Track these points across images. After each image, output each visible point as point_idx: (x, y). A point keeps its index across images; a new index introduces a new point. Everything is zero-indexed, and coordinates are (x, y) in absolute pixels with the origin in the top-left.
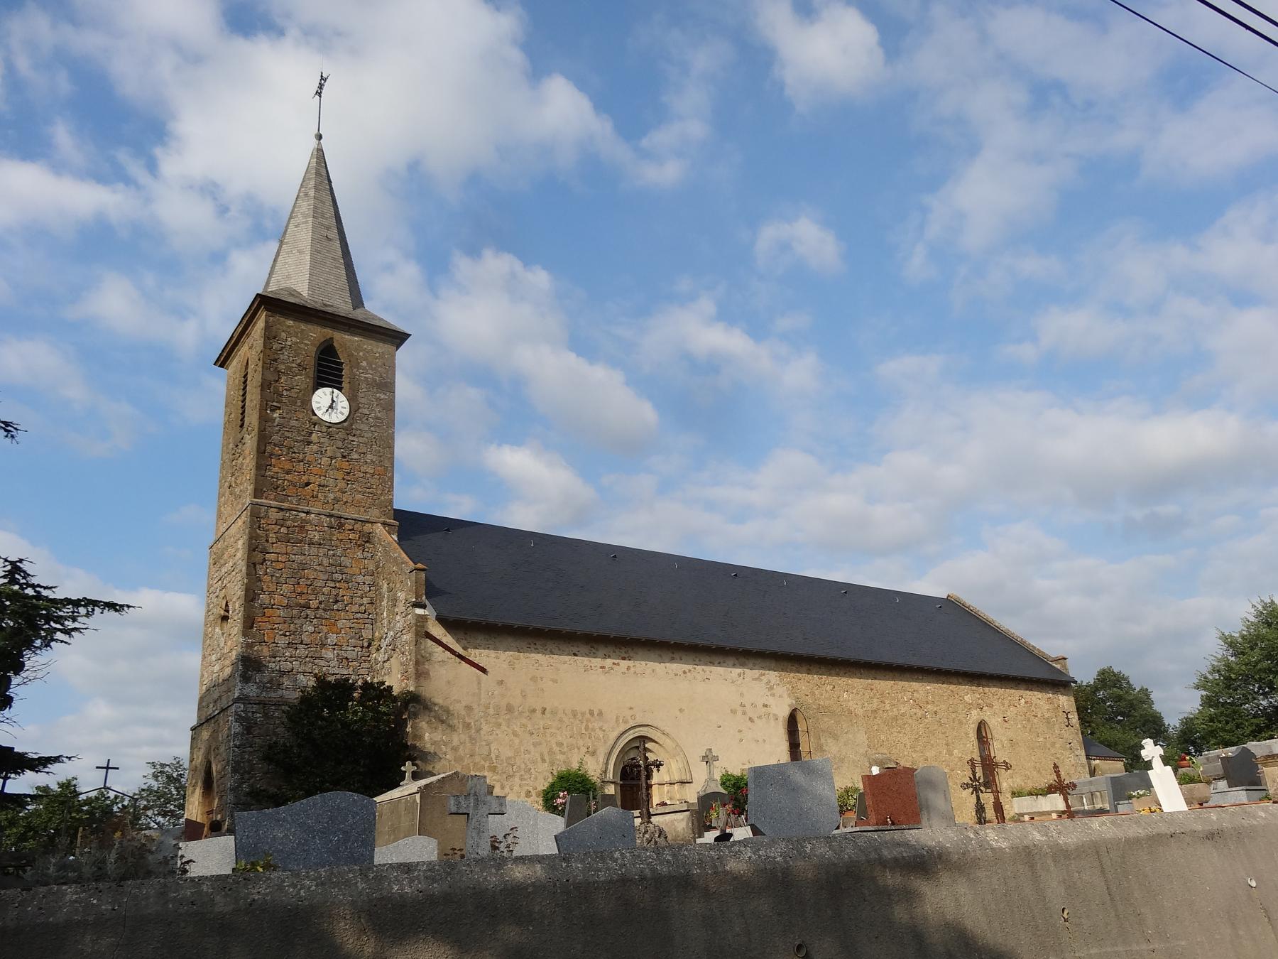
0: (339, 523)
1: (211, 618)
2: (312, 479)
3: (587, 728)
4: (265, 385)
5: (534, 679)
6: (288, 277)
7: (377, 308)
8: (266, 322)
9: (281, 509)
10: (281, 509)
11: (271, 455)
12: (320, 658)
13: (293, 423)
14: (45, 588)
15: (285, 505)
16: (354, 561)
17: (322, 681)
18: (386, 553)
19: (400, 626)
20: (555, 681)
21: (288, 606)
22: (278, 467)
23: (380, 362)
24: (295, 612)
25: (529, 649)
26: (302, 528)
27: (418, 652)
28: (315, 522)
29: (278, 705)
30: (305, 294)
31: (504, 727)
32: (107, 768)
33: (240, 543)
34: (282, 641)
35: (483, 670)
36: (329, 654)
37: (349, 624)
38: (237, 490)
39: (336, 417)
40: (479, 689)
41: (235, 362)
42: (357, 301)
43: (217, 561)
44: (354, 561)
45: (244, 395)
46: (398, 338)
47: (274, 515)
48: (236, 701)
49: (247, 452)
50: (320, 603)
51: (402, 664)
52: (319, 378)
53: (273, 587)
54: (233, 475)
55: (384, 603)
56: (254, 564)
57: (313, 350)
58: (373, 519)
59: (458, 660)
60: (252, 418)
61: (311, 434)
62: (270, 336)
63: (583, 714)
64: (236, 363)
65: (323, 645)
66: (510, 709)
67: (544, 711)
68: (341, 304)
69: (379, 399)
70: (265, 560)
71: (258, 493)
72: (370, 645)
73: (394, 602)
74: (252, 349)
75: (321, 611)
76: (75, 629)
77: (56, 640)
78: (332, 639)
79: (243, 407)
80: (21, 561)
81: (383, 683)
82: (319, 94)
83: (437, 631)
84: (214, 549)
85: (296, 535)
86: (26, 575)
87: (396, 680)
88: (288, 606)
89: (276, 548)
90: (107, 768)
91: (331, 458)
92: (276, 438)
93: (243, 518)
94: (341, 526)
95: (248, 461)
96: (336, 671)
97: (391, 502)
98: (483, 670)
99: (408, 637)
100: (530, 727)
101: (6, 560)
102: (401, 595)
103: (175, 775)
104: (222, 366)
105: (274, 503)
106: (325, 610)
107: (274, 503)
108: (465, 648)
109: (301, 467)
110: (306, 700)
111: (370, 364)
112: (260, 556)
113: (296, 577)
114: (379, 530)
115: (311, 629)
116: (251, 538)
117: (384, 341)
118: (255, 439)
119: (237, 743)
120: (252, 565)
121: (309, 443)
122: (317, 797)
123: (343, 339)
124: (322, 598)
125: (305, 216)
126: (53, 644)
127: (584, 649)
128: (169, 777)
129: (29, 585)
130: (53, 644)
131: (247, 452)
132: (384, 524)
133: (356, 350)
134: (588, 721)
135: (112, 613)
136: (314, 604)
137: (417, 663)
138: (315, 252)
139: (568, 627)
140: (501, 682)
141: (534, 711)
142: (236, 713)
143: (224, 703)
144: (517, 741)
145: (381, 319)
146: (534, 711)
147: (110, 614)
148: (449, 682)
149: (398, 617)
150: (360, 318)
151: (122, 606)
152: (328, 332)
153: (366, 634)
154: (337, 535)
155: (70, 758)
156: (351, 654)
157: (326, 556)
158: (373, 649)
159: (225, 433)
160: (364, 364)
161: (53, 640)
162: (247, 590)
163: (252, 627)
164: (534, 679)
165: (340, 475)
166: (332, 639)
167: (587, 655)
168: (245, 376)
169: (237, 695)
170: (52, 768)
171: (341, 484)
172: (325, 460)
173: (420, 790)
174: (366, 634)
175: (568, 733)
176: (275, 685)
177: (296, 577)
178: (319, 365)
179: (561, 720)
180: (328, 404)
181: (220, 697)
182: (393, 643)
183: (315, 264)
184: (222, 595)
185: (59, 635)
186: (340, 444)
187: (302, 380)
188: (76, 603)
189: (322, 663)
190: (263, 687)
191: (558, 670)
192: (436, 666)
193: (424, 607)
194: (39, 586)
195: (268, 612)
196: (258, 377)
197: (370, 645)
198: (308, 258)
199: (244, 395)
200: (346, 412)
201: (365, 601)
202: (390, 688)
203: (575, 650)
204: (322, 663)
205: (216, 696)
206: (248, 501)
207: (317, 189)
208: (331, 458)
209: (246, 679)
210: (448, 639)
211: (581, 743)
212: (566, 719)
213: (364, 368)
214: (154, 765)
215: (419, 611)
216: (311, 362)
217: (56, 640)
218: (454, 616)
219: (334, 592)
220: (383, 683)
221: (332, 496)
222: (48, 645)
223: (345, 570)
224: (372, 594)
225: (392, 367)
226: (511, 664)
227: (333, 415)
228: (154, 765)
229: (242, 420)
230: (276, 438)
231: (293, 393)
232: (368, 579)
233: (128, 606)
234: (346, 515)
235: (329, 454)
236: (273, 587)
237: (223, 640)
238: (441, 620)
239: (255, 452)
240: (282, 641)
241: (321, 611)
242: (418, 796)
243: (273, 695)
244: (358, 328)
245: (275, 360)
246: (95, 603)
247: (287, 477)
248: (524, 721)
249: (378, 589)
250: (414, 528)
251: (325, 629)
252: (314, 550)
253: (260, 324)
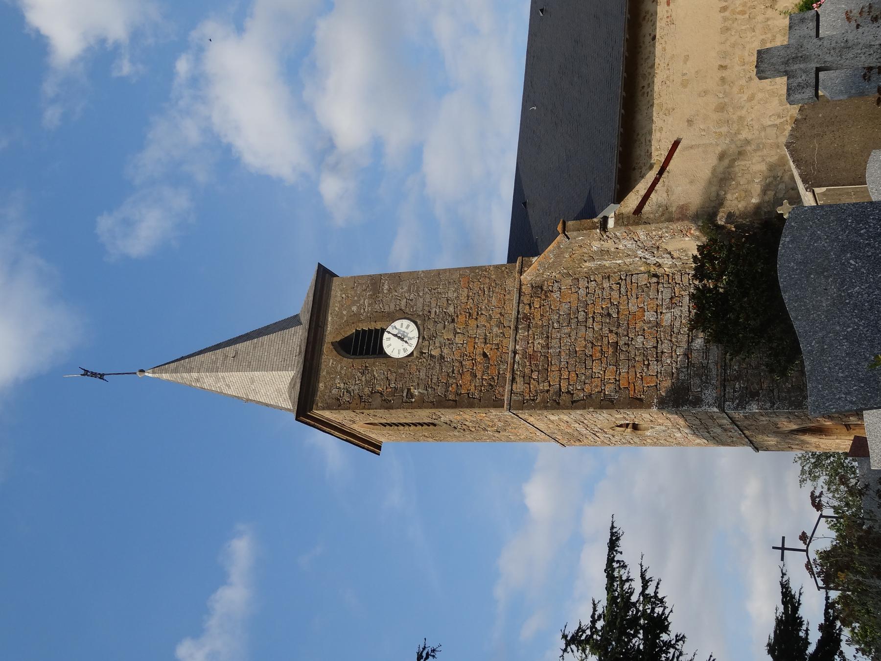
0: (523, 320)
1: (636, 440)
2: (479, 351)
3: (743, 13)
4: (387, 405)
5: (684, 84)
6: (279, 391)
7: (297, 300)
8: (323, 409)
9: (513, 380)
10: (513, 380)
11: (458, 394)
12: (672, 326)
13: (422, 375)
14: (595, 610)
15: (508, 376)
16: (563, 300)
17: (696, 323)
18: (551, 266)
19: (630, 244)
20: (687, 58)
21: (616, 365)
22: (469, 385)
23: (351, 293)
24: (622, 357)
25: (649, 94)
26: (531, 357)
27: (657, 221)
28: (524, 343)
29: (725, 367)
30: (292, 374)
31: (743, 113)
32: (783, 549)
33: (552, 418)
34: (655, 367)
35: (676, 144)
36: (667, 318)
37: (633, 300)
38: (500, 424)
39: (411, 330)
40: (698, 146)
41: (373, 436)
42: (294, 321)
43: (577, 439)
44: (563, 300)
45: (402, 425)
46: (324, 276)
47: (519, 386)
48: (723, 410)
49: (459, 418)
50: (611, 331)
51: (673, 237)
52: (374, 353)
53: (597, 382)
54: (485, 430)
55: (607, 263)
56: (573, 402)
57: (347, 361)
58: (517, 285)
59: (665, 175)
60: (423, 415)
61: (432, 356)
62: (337, 405)
63: (725, 19)
64: (374, 435)
65: (658, 325)
66: (721, 108)
67: (722, 67)
68: (297, 336)
69: (389, 290)
70: (568, 392)
71: (497, 404)
72: (655, 276)
73: (603, 252)
74: (358, 422)
75: (620, 331)
76: (643, 576)
77: (656, 593)
78: (650, 316)
79: (415, 425)
80: (565, 636)
81: (695, 257)
82: (101, 376)
83: (632, 201)
84: (564, 442)
85: (539, 362)
86: (581, 630)
87: (687, 244)
88: (616, 365)
89: (554, 381)
90: (783, 549)
91: (456, 333)
92: (440, 390)
93: (526, 416)
94: (526, 318)
95: (468, 416)
96: (685, 309)
97: (497, 267)
98: (676, 144)
99: (641, 232)
100: (743, 82)
101: (565, 650)
102: (596, 245)
103: (813, 461)
104: (379, 448)
105: (508, 387)
106: (619, 326)
107: (508, 387)
108: (651, 167)
109: (467, 363)
110: (716, 338)
111: (354, 303)
112: (565, 398)
113: (585, 359)
114: (527, 277)
115: (640, 339)
116: (546, 408)
117: (330, 289)
118: (443, 411)
119: (768, 405)
120: (575, 404)
121: (442, 357)
122: (785, 296)
123: (333, 332)
124: (606, 331)
125: (218, 380)
126: (660, 596)
127: (646, 29)
128: (815, 465)
129: (593, 627)
130: (660, 596)
131: (459, 418)
132: (521, 272)
133: (341, 318)
134: (733, 12)
135: (621, 542)
136: (612, 338)
137: (670, 220)
138: (250, 367)
139: (621, 49)
140: (690, 122)
141: (723, 79)
142: (736, 409)
143: (726, 422)
144: (760, 95)
145: (308, 296)
146: (723, 79)
147: (623, 545)
148: (691, 182)
149: (621, 247)
150: (308, 316)
151: (612, 534)
152: (327, 348)
153: (643, 280)
154: (537, 321)
155: (784, 574)
156: (667, 294)
157: (559, 329)
158: (660, 271)
159: (444, 439)
160: (354, 308)
161: (656, 596)
162: (601, 407)
163: (641, 400)
164: (684, 84)
165: (473, 323)
166: (650, 316)
167: (654, 24)
168: (384, 425)
169: (716, 410)
170: (794, 589)
171: (482, 321)
172: (459, 340)
173: (810, 188)
174: (643, 280)
175: (749, 34)
176: (702, 372)
177: (585, 359)
178: (361, 354)
179: (733, 46)
180: (400, 341)
181: (720, 426)
182: (650, 250)
183: (261, 366)
184: (611, 432)
185: (650, 591)
186: (440, 326)
187: (378, 369)
188: (611, 578)
189: (677, 324)
190: (705, 384)
191: (673, 56)
192: (673, 198)
193: (605, 219)
194: (593, 616)
195: (623, 384)
196: (380, 412)
197: (655, 276)
198: (257, 373)
199: (402, 425)
200: (406, 322)
201: (606, 285)
202: (700, 248)
203: (648, 39)
204: (677, 324)
205: (719, 430)
206: (507, 413)
207: (190, 371)
208: (456, 333)
209: (697, 402)
210: (642, 187)
211: (760, 18)
212: (733, 40)
213: (359, 308)
214: (802, 481)
215: (611, 223)
216: (358, 362)
217: (656, 593)
218: (613, 184)
219: (598, 318)
220: (695, 257)
221: (495, 329)
222: (662, 601)
223: (574, 309)
224: (599, 278)
225: (355, 279)
226: (669, 112)
227: (410, 335)
228: (802, 481)
229: (428, 424)
230: (440, 390)
231: (392, 377)
232: (583, 283)
233: (613, 527)
234: (514, 313)
235: (451, 336)
236: (597, 382)
237: (658, 428)
238: (619, 198)
239: (457, 411)
240: (655, 367)
241: (620, 331)
242: (818, 190)
243: (714, 372)
244: (318, 317)
245: (361, 397)
246: (610, 560)
247: (479, 376)
248: (735, 90)
249: (592, 271)
250: (525, 242)
251: (640, 324)
252: (554, 343)
253: (327, 415)
